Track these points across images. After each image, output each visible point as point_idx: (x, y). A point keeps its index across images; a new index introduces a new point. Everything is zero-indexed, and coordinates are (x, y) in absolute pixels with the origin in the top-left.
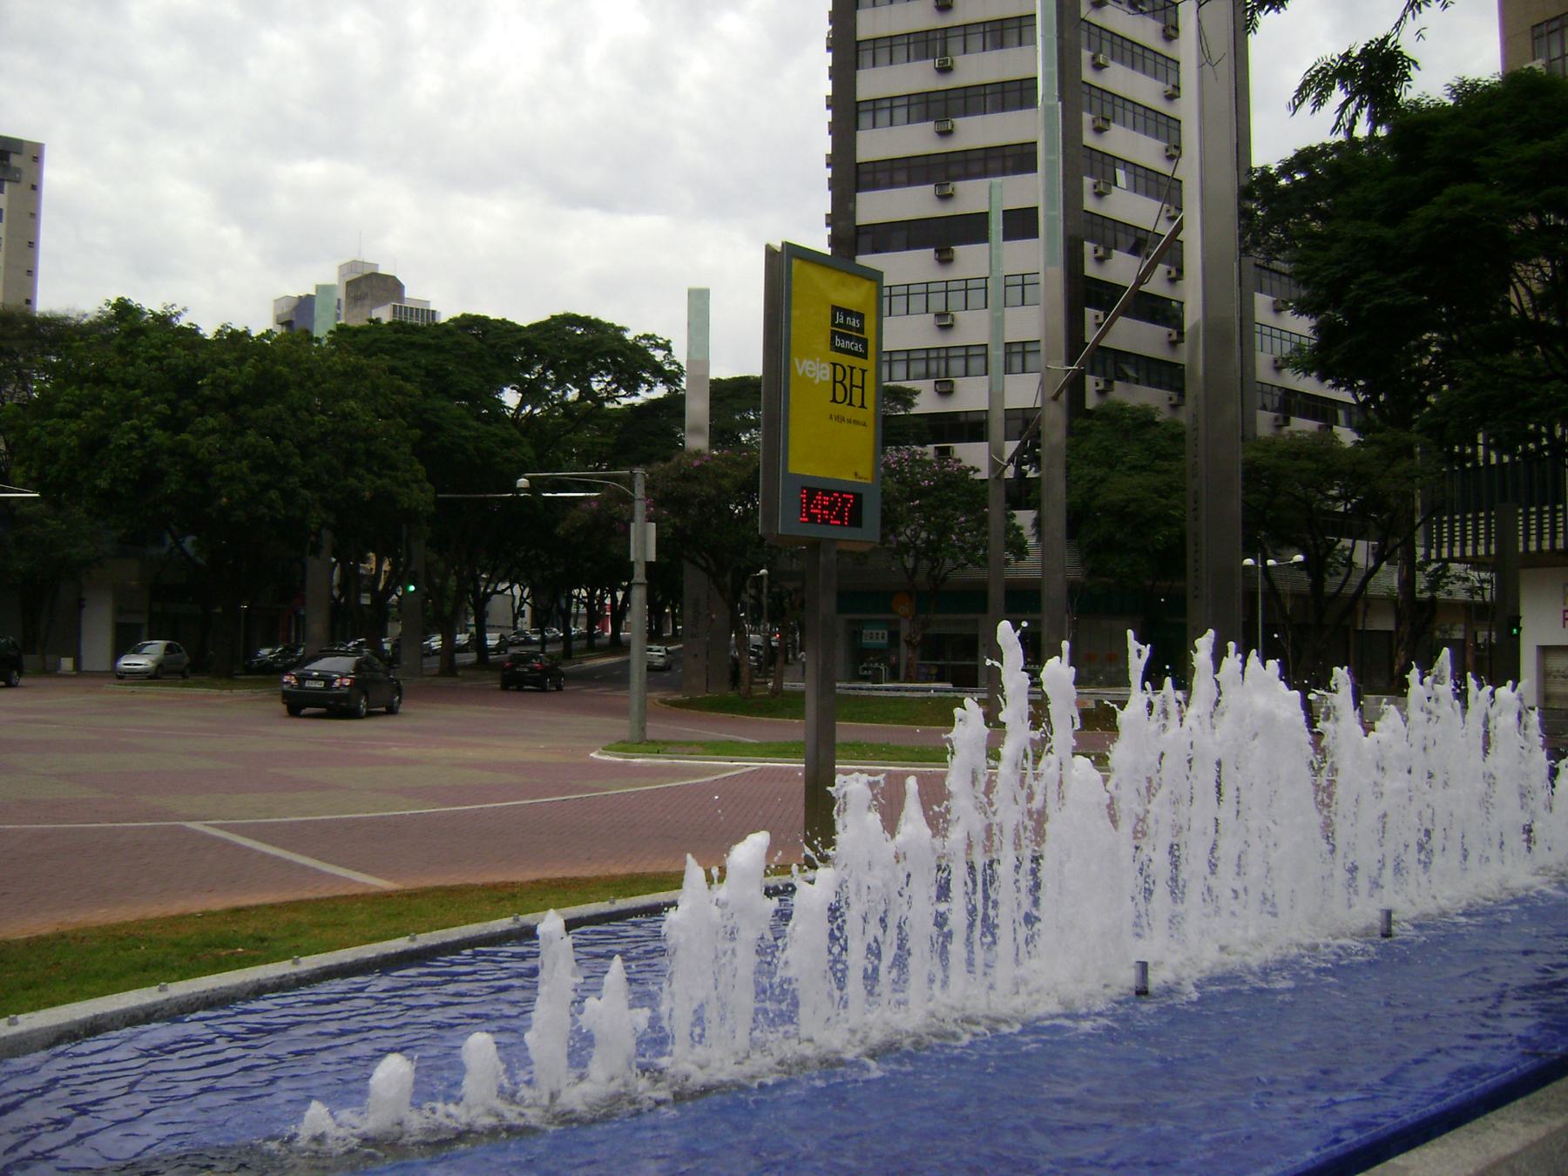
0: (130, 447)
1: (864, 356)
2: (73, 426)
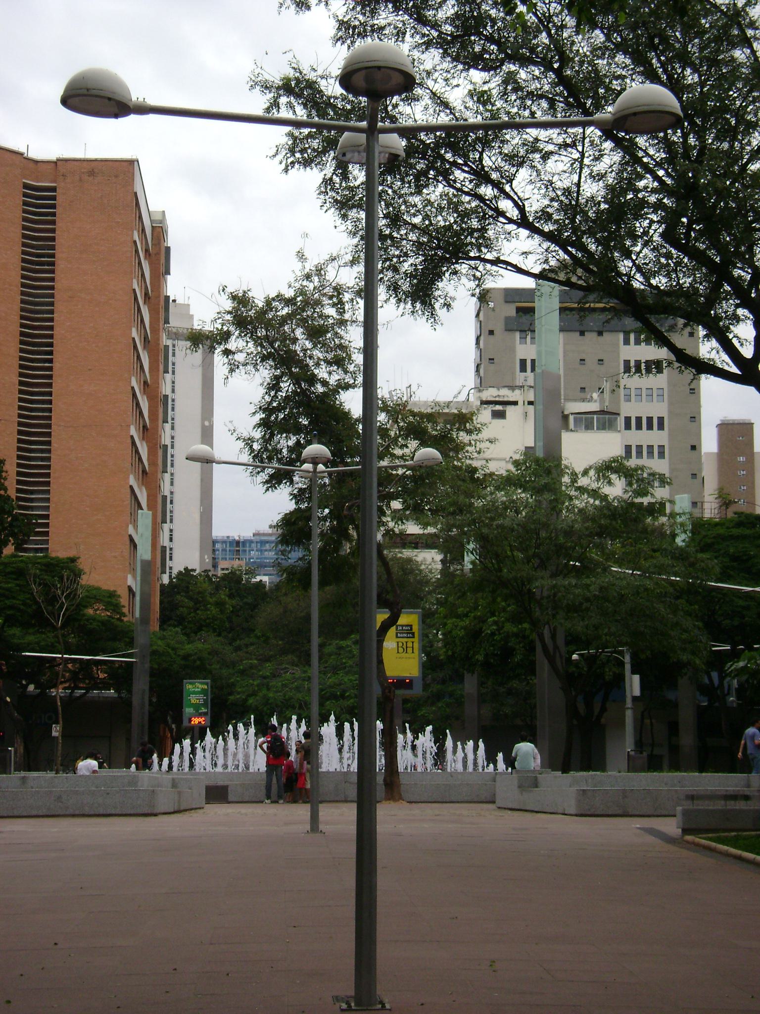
0: (493, 634)
1: (413, 637)
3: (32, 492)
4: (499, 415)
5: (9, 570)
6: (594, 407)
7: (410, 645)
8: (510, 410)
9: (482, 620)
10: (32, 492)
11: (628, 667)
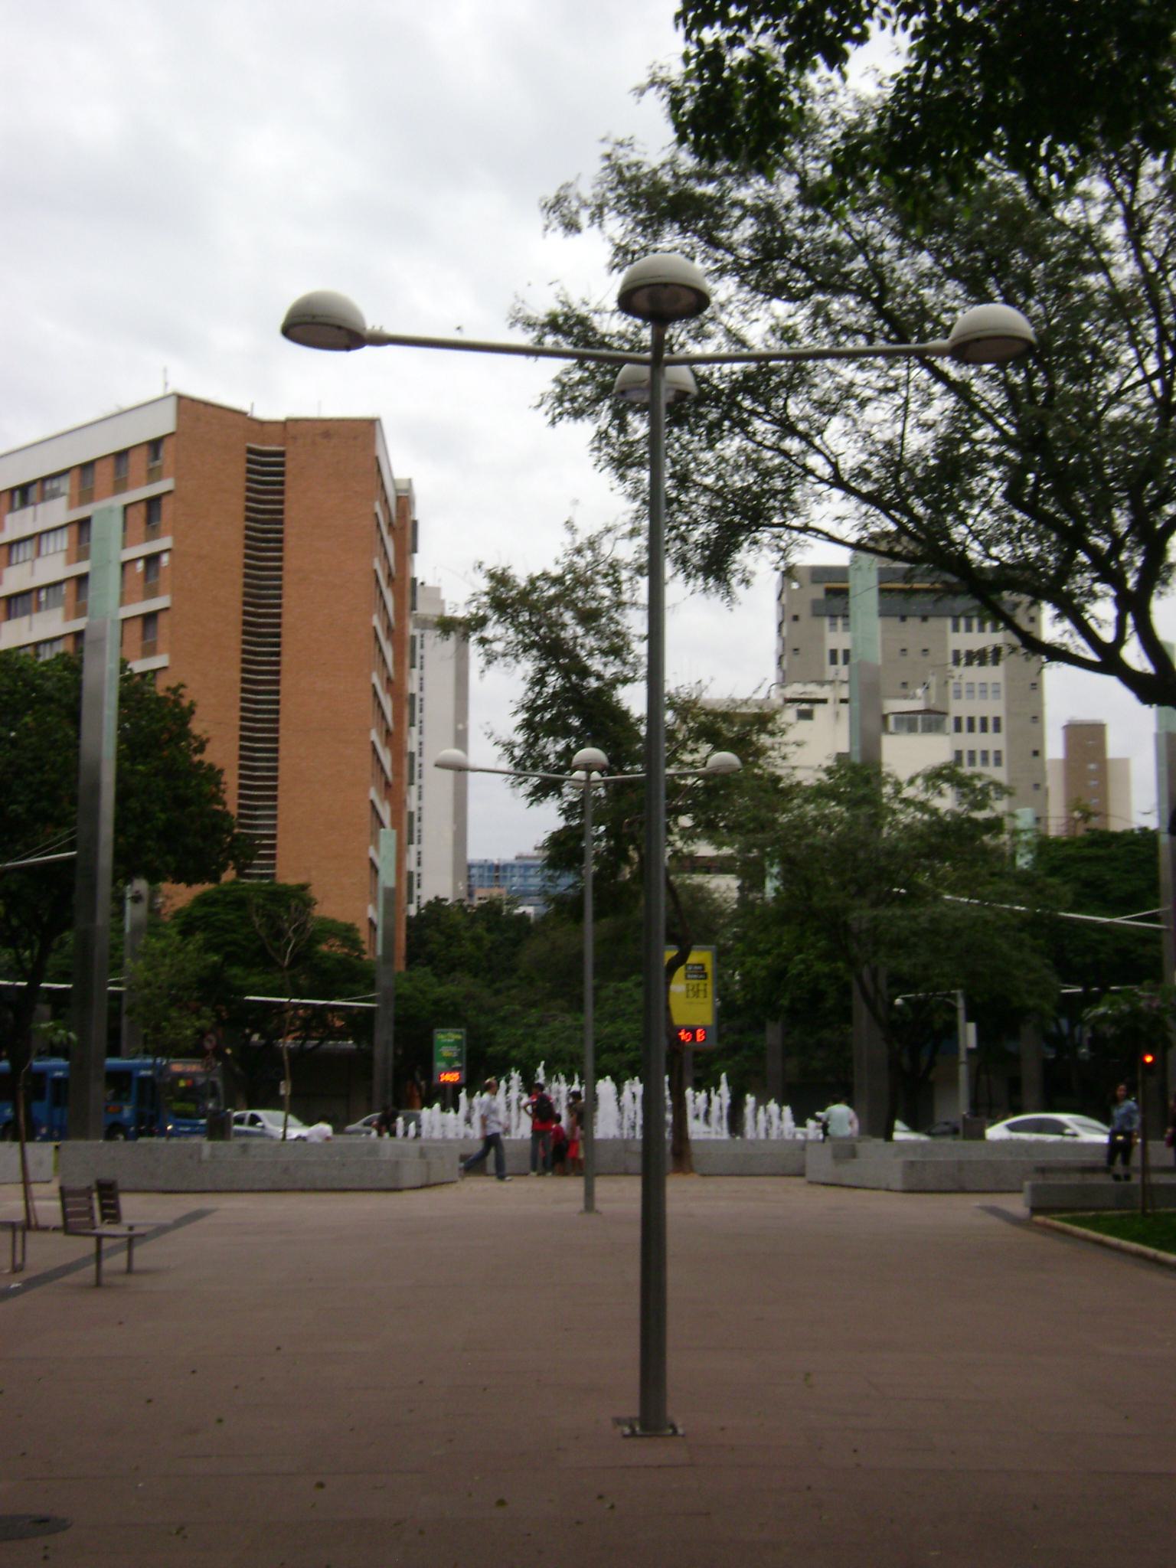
0: (800, 975)
2: (762, 962)
3: (256, 808)
4: (806, 715)
5: (228, 899)
6: (917, 705)
7: (701, 987)
8: (818, 709)
9: (788, 958)
10: (256, 808)
11: (961, 1014)
